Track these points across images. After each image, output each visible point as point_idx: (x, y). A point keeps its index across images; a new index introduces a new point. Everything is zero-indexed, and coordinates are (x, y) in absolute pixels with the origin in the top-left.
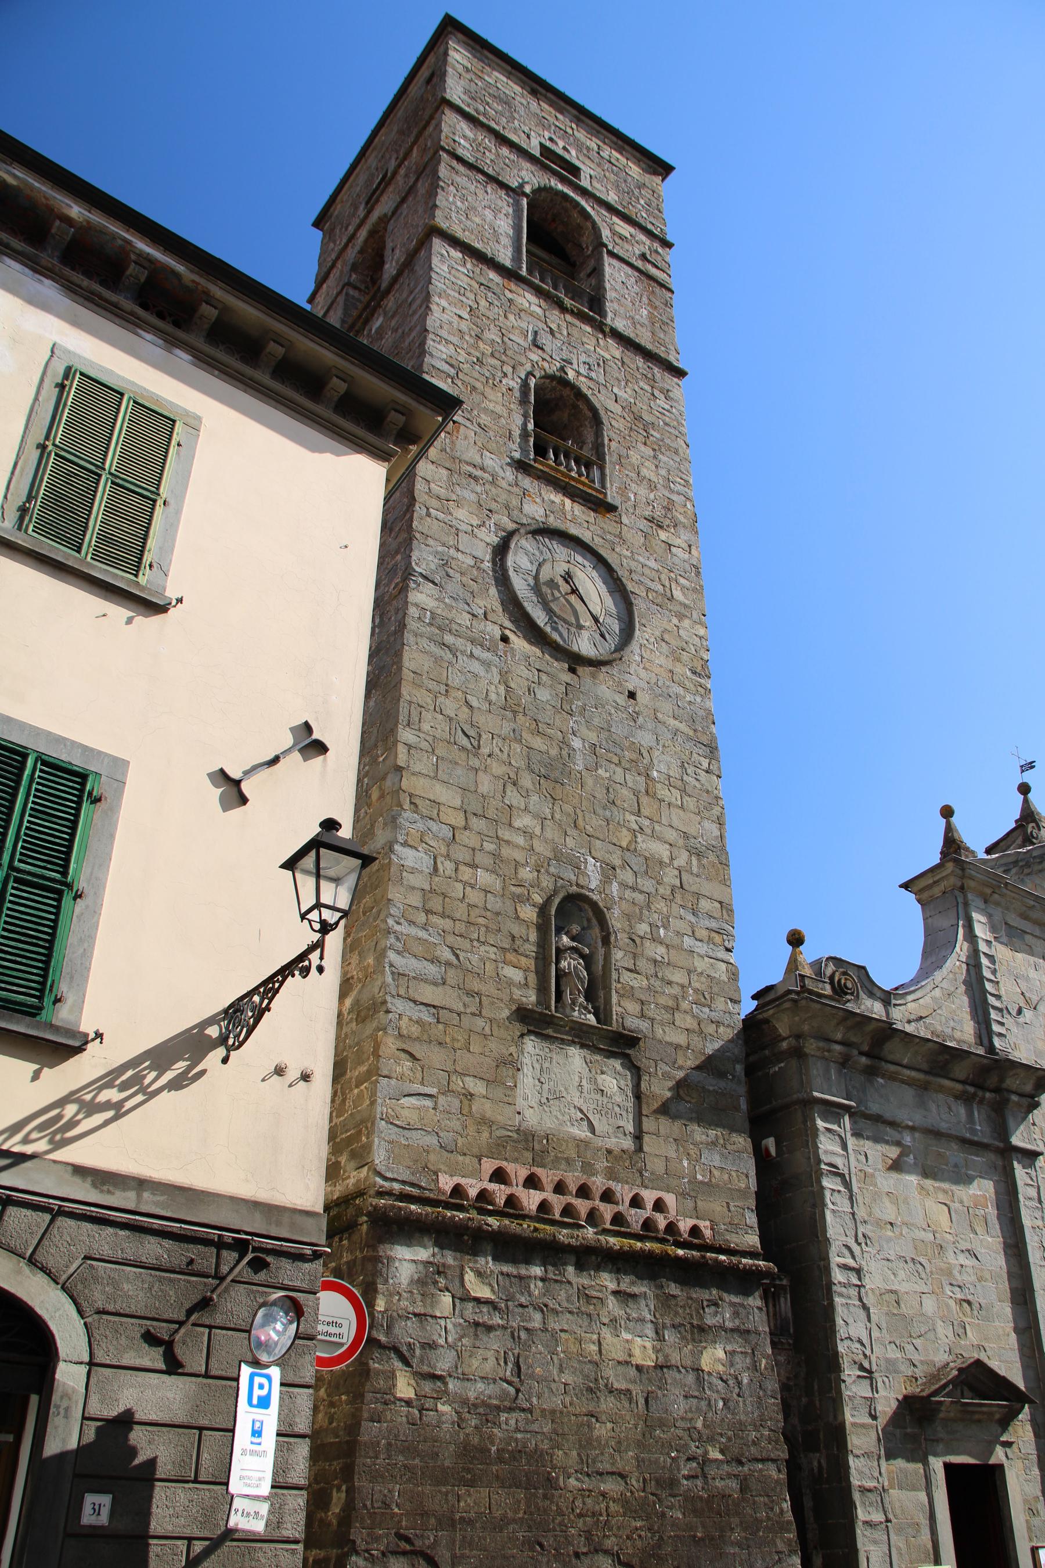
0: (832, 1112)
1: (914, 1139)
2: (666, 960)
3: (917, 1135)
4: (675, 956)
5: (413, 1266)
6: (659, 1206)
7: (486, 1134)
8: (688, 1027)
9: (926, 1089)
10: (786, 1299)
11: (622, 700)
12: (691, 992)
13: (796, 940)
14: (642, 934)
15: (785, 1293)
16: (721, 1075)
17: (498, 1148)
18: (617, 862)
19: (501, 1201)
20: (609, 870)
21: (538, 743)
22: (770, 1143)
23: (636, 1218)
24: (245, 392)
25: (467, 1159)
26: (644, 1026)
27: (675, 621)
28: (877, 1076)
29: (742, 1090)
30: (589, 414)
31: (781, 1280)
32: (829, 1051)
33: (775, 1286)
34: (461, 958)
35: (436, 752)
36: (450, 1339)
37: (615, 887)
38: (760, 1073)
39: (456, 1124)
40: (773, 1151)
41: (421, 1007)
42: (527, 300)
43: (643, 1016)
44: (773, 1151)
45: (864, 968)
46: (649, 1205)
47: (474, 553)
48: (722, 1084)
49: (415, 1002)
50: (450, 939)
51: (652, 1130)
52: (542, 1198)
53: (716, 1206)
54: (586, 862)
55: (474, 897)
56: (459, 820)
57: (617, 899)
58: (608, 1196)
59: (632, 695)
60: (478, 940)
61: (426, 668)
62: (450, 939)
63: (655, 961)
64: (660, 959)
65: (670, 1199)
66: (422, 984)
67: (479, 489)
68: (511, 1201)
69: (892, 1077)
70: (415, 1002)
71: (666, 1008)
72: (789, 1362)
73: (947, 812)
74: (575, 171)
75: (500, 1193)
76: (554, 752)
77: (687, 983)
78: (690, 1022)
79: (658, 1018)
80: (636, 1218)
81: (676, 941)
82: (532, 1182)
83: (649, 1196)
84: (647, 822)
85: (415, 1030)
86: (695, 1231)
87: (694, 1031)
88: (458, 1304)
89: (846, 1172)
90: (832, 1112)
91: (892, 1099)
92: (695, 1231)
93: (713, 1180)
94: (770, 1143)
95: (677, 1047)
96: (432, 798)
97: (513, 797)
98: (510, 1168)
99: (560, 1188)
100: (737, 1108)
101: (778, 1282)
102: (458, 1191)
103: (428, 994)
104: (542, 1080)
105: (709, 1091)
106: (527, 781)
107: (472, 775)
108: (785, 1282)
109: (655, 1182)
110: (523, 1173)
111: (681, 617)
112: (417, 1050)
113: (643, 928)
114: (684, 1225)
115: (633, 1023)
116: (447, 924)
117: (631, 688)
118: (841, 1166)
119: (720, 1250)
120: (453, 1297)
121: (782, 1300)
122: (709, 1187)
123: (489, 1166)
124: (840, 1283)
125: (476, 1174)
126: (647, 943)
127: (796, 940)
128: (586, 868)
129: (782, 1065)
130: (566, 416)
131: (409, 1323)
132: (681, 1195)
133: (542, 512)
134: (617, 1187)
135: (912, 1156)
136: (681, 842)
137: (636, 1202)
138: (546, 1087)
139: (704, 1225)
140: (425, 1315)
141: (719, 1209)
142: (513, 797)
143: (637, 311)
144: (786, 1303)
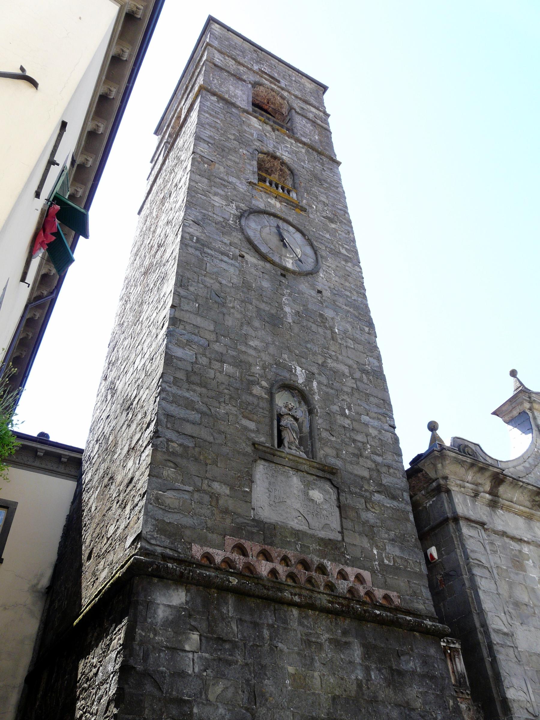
0: (472, 526)
1: (530, 551)
2: (351, 427)
3: (531, 547)
4: (356, 425)
5: (168, 611)
6: (359, 578)
7: (228, 521)
8: (370, 467)
9: (531, 519)
10: (460, 660)
11: (313, 293)
12: (369, 447)
13: (433, 427)
14: (335, 411)
15: (459, 655)
16: (394, 498)
17: (237, 531)
18: (316, 371)
19: (240, 566)
20: (310, 377)
21: (263, 306)
22: (433, 551)
23: (343, 586)
24: (67, 479)
25: (215, 536)
26: (338, 463)
27: (343, 263)
28: (498, 508)
29: (409, 508)
30: (288, 172)
31: (454, 643)
32: (464, 487)
33: (450, 648)
34: (212, 411)
35: (198, 301)
36: (196, 670)
37: (315, 384)
38: (420, 508)
39: (208, 512)
40: (435, 555)
41: (183, 436)
42: (254, 122)
43: (338, 456)
44: (435, 555)
45: (478, 445)
46: (352, 578)
47: (224, 216)
48: (395, 503)
49: (178, 432)
50: (206, 399)
51: (350, 527)
52: (272, 567)
53: (402, 583)
54: (295, 369)
55: (221, 378)
56: (212, 337)
57: (316, 391)
58: (322, 569)
59: (319, 292)
60: (224, 402)
61: (193, 262)
62: (206, 399)
63: (344, 427)
64: (347, 426)
65: (367, 575)
66: (184, 422)
67: (226, 190)
68: (249, 567)
69: (509, 509)
70: (178, 432)
71: (354, 455)
72: (470, 710)
73: (513, 373)
74: (279, 82)
75: (239, 560)
76: (273, 311)
77: (366, 441)
78: (370, 464)
79: (348, 459)
80: (343, 586)
81: (357, 417)
82: (266, 556)
83: (351, 572)
84: (334, 354)
85: (179, 449)
86: (386, 597)
87: (373, 470)
88: (204, 641)
89: (489, 566)
90: (472, 526)
91: (510, 524)
92: (386, 597)
93: (396, 564)
94: (433, 551)
95: (363, 478)
96: (195, 324)
97: (246, 329)
98: (247, 544)
99: (285, 560)
100: (408, 520)
101: (452, 646)
102: (208, 556)
103: (189, 429)
104: (270, 489)
105: (387, 507)
106: (257, 323)
107: (221, 316)
108: (457, 646)
109: (353, 563)
110: (257, 548)
111: (346, 261)
112: (178, 460)
113: (335, 408)
114: (379, 593)
115: (332, 461)
116: (204, 390)
117: (320, 289)
118: (484, 561)
119: (408, 612)
120: (200, 636)
121: (457, 660)
122: (395, 570)
123: (230, 541)
124: (498, 643)
125: (221, 546)
126: (338, 417)
127: (433, 427)
128: (295, 372)
129: (434, 499)
130: (277, 176)
131: (162, 655)
132: (373, 572)
133: (263, 205)
134: (328, 564)
135: (531, 561)
136: (355, 366)
137: (343, 575)
138: (273, 494)
139: (393, 595)
140: (174, 649)
141: (402, 584)
142: (246, 329)
143: (313, 136)
144: (460, 663)
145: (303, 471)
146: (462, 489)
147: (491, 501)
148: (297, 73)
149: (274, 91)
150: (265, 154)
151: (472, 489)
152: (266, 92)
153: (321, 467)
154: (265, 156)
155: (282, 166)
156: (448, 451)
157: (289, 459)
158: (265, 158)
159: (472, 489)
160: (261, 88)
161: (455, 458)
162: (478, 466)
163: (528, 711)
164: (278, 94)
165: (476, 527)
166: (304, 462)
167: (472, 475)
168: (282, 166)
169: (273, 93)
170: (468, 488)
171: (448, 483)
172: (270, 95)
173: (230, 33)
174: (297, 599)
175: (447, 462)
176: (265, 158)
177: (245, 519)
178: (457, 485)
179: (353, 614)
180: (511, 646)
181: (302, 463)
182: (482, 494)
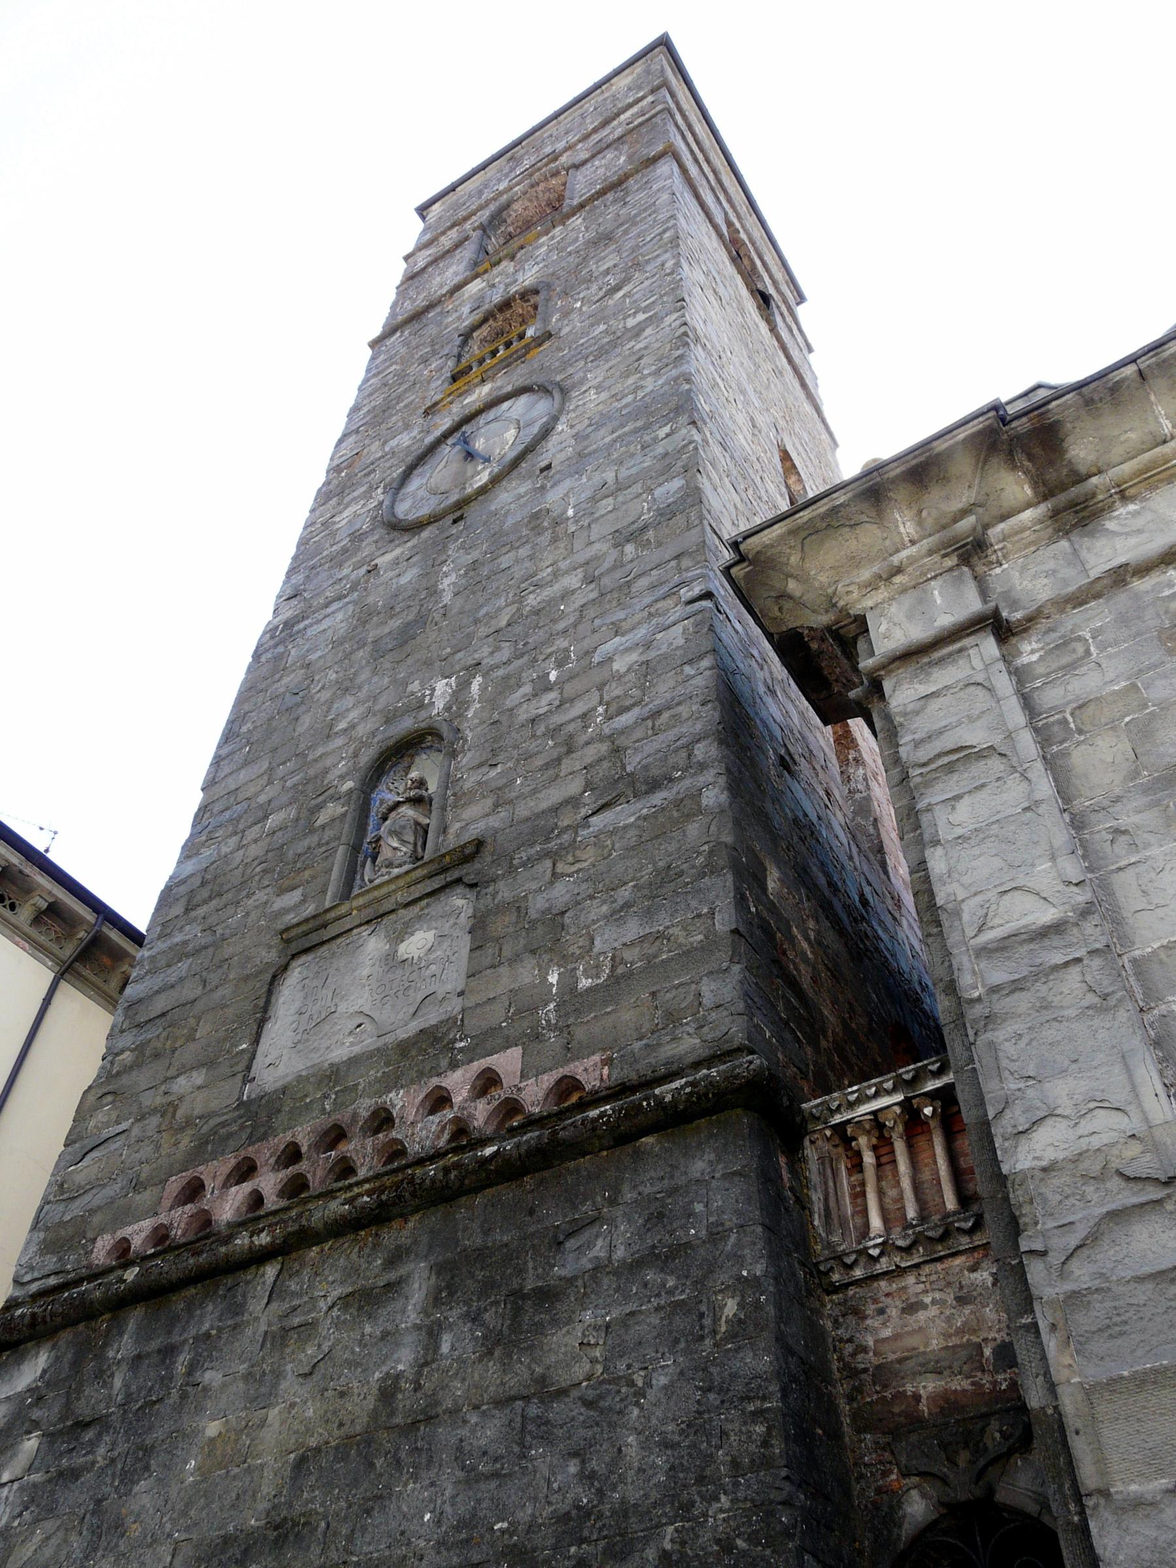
28: (1111, 508)
32: (899, 570)
89: (996, 739)
145: (393, 911)
146: (898, 579)
147: (1055, 514)
148: (599, 91)
149: (538, 184)
150: (485, 320)
151: (931, 552)
152: (531, 201)
153: (433, 867)
154: (491, 322)
155: (528, 301)
156: (749, 541)
157: (359, 909)
158: (495, 325)
159: (931, 552)
160: (515, 206)
161: (793, 532)
162: (893, 481)
163: (1128, 1179)
164: (546, 179)
165: (961, 650)
166: (393, 887)
167: (909, 514)
168: (528, 301)
169: (542, 186)
170: (912, 560)
171: (841, 603)
172: (541, 195)
173: (459, 189)
174: (264, 1239)
175: (794, 560)
176: (495, 325)
177: (224, 1114)
178: (871, 586)
179: (413, 1195)
180: (1066, 964)
181: (388, 895)
182: (991, 532)
